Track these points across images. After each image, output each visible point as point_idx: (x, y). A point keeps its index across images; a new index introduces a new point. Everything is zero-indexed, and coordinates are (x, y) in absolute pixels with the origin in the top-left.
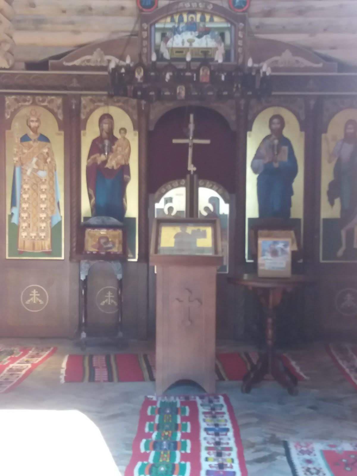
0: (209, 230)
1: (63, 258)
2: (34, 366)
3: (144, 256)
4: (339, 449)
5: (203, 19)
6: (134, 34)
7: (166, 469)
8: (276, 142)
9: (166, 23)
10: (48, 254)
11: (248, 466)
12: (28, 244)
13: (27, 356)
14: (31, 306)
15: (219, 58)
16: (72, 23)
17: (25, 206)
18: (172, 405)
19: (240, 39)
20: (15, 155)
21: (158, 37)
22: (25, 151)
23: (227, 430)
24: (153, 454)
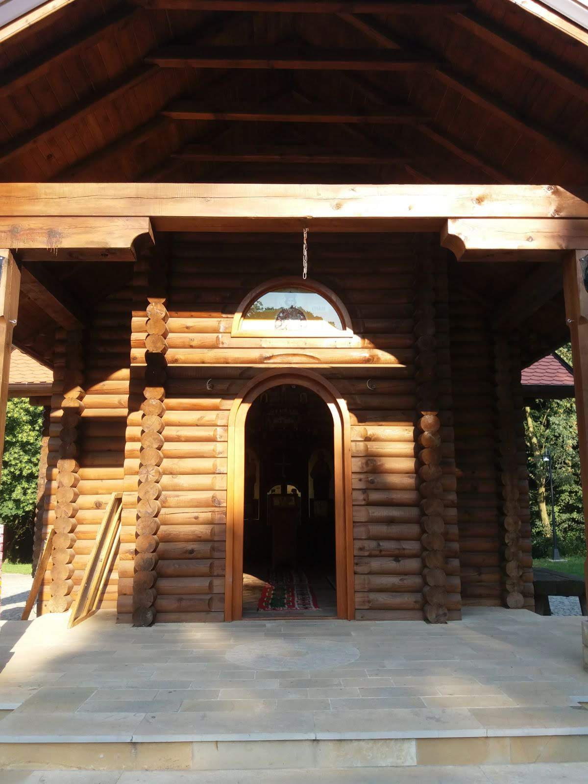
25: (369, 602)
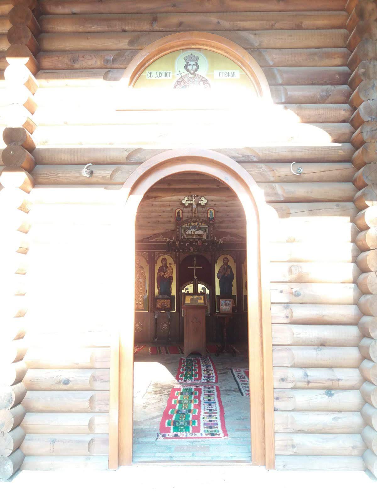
0: (202, 297)
3: (178, 310)
5: (198, 224)
6: (174, 230)
9: (185, 226)
15: (205, 237)
18: (190, 360)
21: (183, 230)
24: (185, 372)
25: (293, 446)
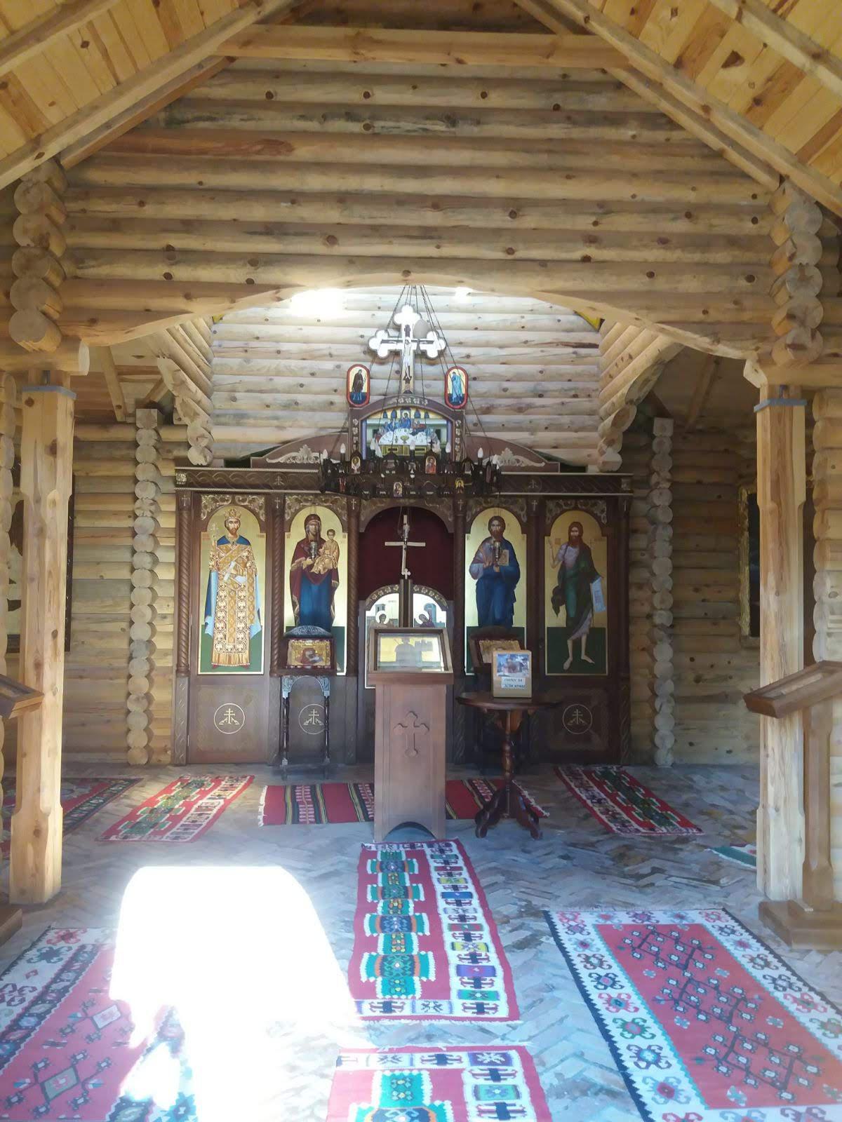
1: (262, 673)
2: (228, 802)
3: (354, 670)
4: (616, 921)
6: (345, 430)
7: (403, 965)
8: (497, 544)
9: (376, 420)
10: (246, 668)
11: (508, 955)
12: (223, 657)
13: (219, 788)
14: (226, 727)
16: (277, 418)
17: (220, 615)
19: (457, 436)
20: (212, 559)
21: (370, 432)
22: (222, 555)
23: (470, 895)
